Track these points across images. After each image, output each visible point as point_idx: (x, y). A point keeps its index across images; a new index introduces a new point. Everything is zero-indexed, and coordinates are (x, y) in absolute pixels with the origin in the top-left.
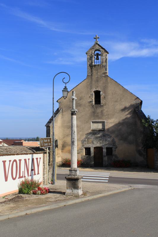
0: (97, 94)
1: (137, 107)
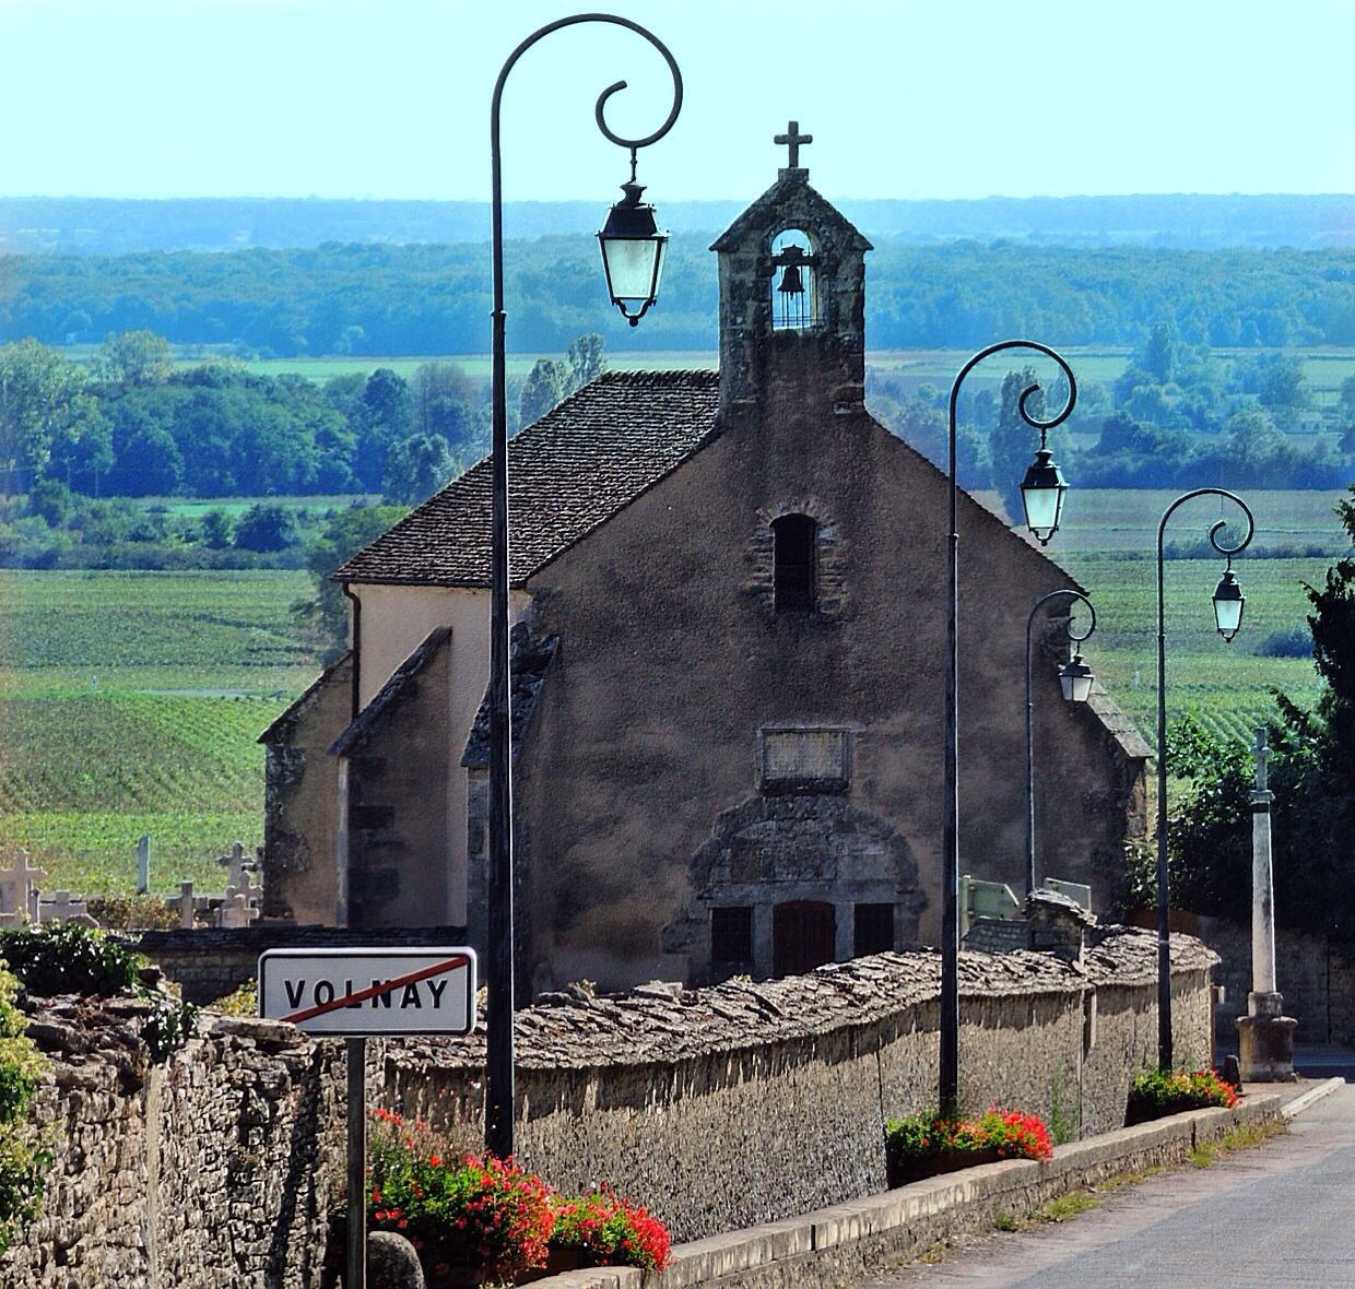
0: (795, 537)
1: (1053, 636)
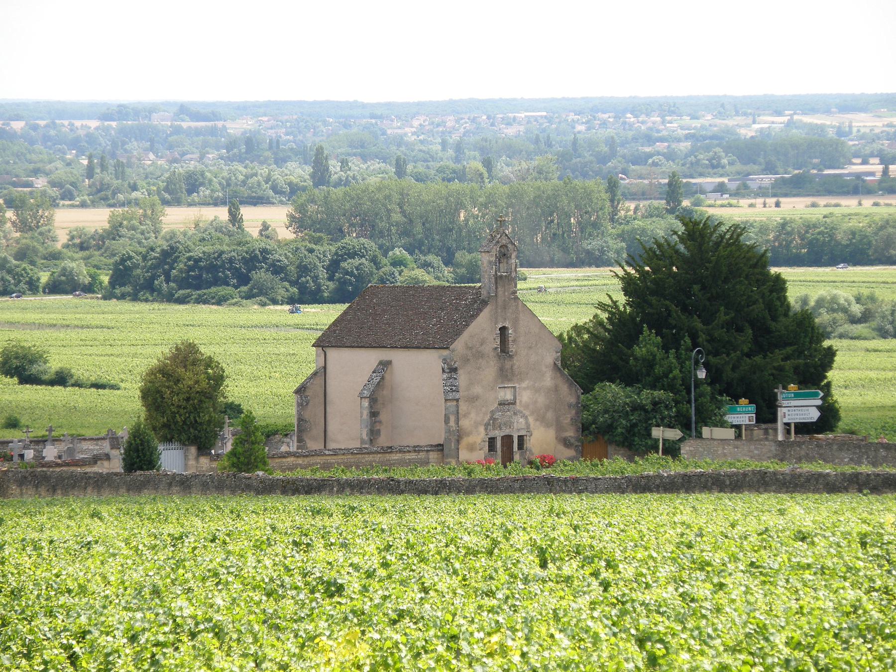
0: (503, 330)
